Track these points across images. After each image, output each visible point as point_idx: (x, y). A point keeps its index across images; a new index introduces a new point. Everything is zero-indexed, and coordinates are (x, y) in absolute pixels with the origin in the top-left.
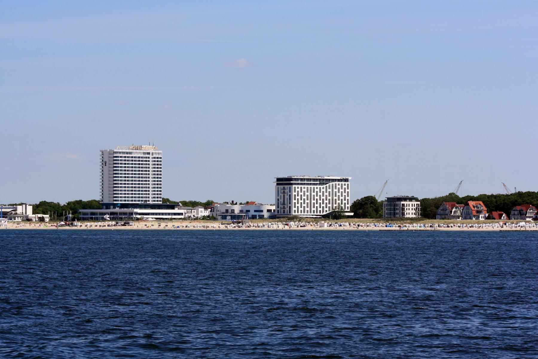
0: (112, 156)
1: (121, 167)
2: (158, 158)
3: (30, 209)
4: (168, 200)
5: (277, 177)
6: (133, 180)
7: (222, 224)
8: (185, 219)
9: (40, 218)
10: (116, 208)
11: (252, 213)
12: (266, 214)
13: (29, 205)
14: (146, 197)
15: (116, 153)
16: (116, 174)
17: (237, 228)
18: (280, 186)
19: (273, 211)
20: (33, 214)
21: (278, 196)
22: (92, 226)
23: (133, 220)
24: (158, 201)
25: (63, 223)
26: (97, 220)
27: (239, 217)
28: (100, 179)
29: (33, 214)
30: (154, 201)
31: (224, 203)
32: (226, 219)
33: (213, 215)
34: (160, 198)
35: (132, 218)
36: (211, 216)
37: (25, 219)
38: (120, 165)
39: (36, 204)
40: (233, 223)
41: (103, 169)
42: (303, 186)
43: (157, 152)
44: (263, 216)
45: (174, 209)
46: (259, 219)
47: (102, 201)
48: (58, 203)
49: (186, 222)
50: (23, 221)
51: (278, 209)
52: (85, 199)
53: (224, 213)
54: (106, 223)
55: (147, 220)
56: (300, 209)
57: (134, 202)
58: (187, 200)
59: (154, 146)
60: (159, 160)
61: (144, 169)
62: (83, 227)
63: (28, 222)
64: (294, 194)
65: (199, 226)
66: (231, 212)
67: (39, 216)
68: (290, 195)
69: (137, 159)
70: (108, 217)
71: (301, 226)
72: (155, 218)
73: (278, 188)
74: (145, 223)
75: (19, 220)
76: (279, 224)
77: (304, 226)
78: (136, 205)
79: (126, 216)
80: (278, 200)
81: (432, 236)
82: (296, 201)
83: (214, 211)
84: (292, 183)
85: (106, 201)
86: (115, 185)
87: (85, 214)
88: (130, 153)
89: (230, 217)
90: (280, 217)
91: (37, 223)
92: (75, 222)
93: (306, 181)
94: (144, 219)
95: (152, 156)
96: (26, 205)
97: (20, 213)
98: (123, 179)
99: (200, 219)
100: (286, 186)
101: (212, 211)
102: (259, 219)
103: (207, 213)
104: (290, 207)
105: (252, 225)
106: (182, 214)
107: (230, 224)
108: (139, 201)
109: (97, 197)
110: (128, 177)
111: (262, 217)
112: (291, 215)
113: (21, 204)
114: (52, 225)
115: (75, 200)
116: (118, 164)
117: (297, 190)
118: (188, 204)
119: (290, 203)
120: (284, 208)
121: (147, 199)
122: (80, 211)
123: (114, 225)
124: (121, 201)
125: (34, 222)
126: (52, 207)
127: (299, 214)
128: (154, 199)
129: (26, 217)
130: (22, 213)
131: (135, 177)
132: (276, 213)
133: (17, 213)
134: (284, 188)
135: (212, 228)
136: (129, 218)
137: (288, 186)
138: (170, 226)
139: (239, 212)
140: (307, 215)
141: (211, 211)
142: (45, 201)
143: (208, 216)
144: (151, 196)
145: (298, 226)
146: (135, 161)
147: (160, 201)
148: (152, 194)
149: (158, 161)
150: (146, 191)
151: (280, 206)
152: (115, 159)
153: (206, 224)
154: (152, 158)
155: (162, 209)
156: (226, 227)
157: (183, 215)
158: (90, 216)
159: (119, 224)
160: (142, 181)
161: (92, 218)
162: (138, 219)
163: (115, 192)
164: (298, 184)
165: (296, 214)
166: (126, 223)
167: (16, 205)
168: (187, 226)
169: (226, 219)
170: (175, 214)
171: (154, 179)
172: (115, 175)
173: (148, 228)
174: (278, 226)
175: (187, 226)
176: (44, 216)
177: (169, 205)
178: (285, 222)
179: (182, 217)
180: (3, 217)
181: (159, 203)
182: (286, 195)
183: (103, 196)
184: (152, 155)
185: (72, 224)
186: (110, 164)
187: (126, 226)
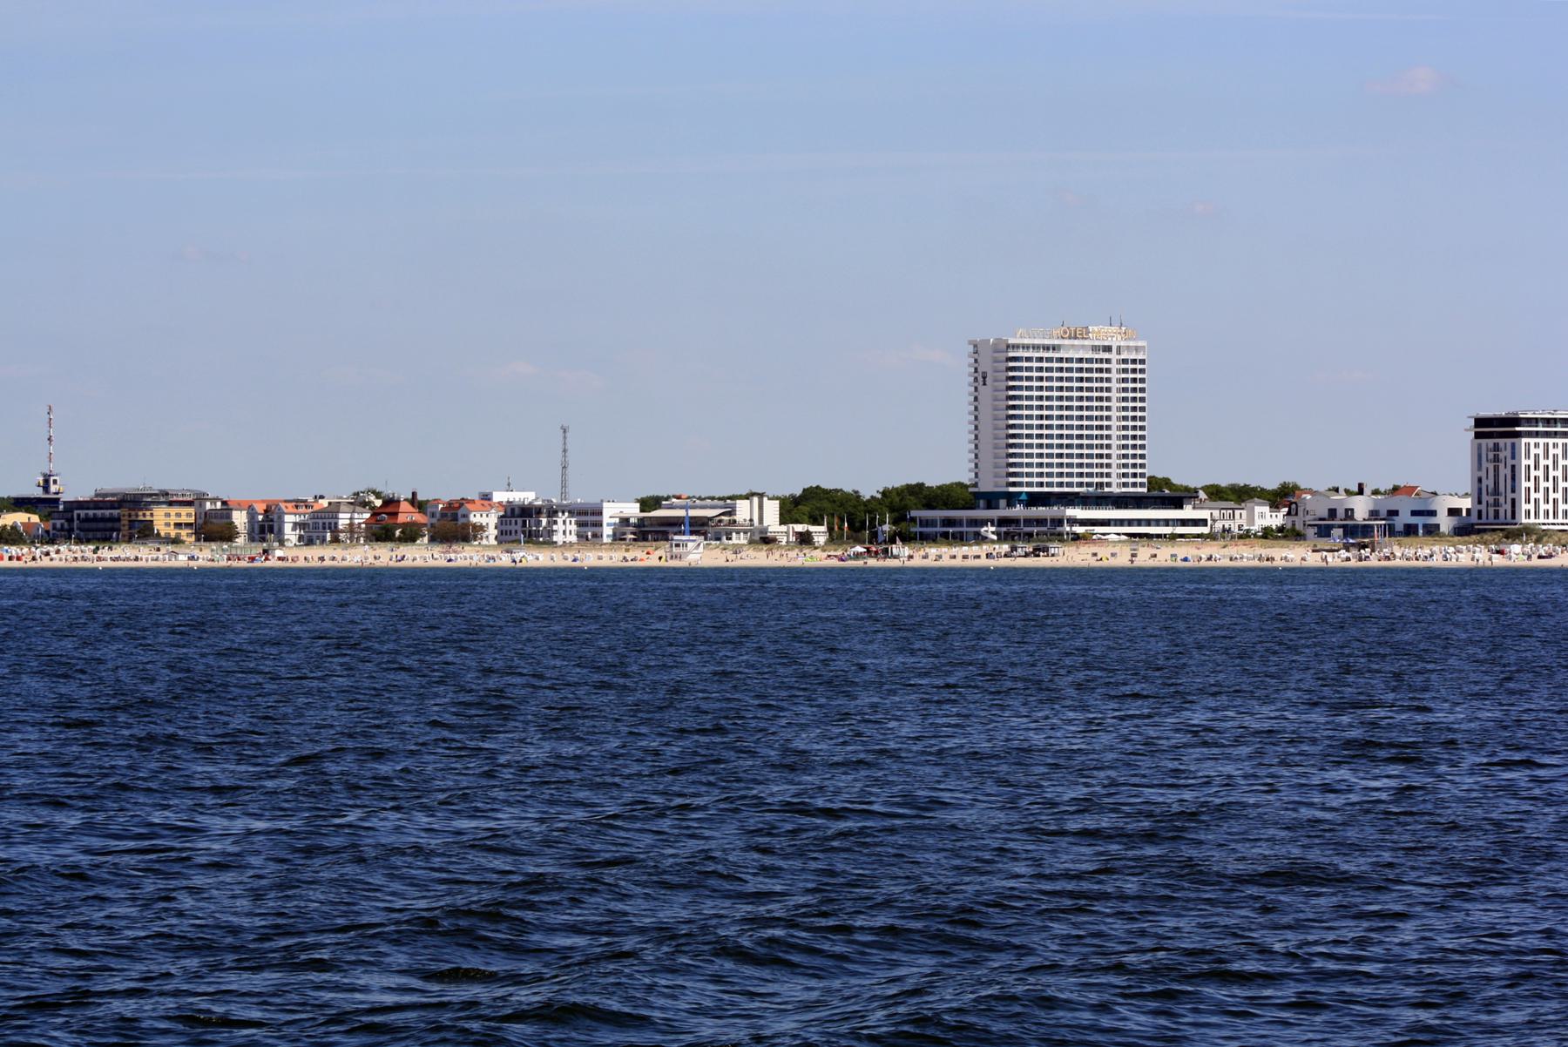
0: (1002, 356)
1: (1029, 388)
2: (1134, 361)
3: (772, 510)
4: (1166, 482)
5: (1475, 415)
6: (1062, 416)
7: (1314, 551)
8: (1212, 537)
9: (800, 534)
11: (1405, 518)
12: (1445, 523)
13: (769, 499)
14: (1102, 475)
15: (1015, 347)
16: (1014, 407)
17: (1353, 563)
18: (1484, 442)
19: (1464, 514)
20: (782, 522)
21: (1480, 468)
22: (940, 557)
23: (1062, 541)
24: (1134, 485)
25: (859, 549)
26: (962, 539)
27: (1366, 530)
28: (970, 423)
29: (782, 522)
30: (1125, 485)
31: (1330, 490)
32: (1329, 535)
33: (1294, 525)
34: (1142, 475)
35: (1060, 534)
36: (1289, 526)
37: (757, 537)
38: (1025, 393)
39: (792, 496)
40: (1347, 548)
41: (976, 394)
42: (1551, 441)
43: (1132, 343)
44: (1438, 526)
46: (1424, 535)
47: (976, 485)
48: (856, 492)
49: (1211, 546)
50: (751, 542)
51: (1480, 507)
52: (933, 481)
53: (1324, 519)
54: (986, 548)
55: (1102, 541)
56: (1543, 507)
57: (1066, 490)
58: (1224, 483)
59: (1123, 328)
60: (1139, 366)
61: (1095, 394)
62: (917, 562)
63: (765, 547)
64: (1524, 462)
65: (1247, 556)
66: (1343, 516)
67: (796, 530)
68: (1513, 467)
69: (1075, 365)
70: (993, 533)
71: (1540, 557)
73: (1480, 447)
74: (1094, 549)
75: (742, 540)
76: (1477, 549)
77: (1550, 556)
78: (1072, 497)
79: (1044, 529)
80: (1480, 480)
82: (1531, 484)
83: (1296, 514)
84: (1520, 432)
85: (986, 486)
86: (1011, 441)
88: (1054, 349)
89: (1341, 530)
90: (1485, 531)
91: (791, 549)
93: (1559, 425)
94: (1094, 537)
95: (1118, 357)
97: (745, 520)
98: (1035, 422)
99: (1255, 535)
100: (1501, 441)
101: (1293, 512)
102: (1424, 535)
103: (1276, 519)
104: (1513, 501)
105: (1398, 554)
106: (1203, 522)
107: (1337, 551)
108: (1080, 485)
109: (959, 472)
110: (1048, 417)
111: (1432, 531)
112: (1516, 524)
113: (748, 497)
114: (829, 556)
115: (904, 483)
116: (1020, 379)
117: (1531, 450)
119: (1513, 491)
120: (1496, 504)
121: (1105, 480)
122: (914, 513)
123: (1006, 556)
124: (1029, 484)
125: (781, 547)
126: (838, 503)
127: (1542, 520)
128: (1124, 480)
129: (761, 532)
130: (751, 520)
131: (1069, 418)
132: (1474, 519)
133: (735, 521)
134: (1496, 448)
135: (1284, 564)
136: (1053, 531)
137: (1509, 441)
138: (1163, 556)
139: (1367, 516)
140: (1563, 524)
141: (1289, 513)
142: (818, 487)
143: (1281, 529)
144: (1114, 471)
145: (1529, 557)
146: (1069, 370)
147: (1142, 485)
148: (1119, 466)
149: (1134, 399)
150: (1101, 428)
151: (1485, 498)
152: (1011, 364)
153: (1265, 552)
154: (1118, 362)
155: (1146, 507)
156: (1325, 559)
157: (1206, 525)
158: (939, 529)
159: (1019, 550)
160: (1088, 428)
161: (945, 535)
163: (1011, 460)
164: (1537, 434)
165: (1532, 520)
166: (1039, 550)
167: (733, 498)
168: (1211, 557)
169: (1329, 535)
170: (1184, 523)
171: (1124, 414)
173: (1099, 564)
174: (1474, 555)
175: (1211, 557)
176: (812, 528)
177: (1166, 495)
178: (1496, 544)
179: (1205, 530)
180: (692, 533)
182: (1502, 466)
183: (977, 470)
184: (1119, 352)
185: (886, 551)
186: (996, 381)
187: (1039, 556)
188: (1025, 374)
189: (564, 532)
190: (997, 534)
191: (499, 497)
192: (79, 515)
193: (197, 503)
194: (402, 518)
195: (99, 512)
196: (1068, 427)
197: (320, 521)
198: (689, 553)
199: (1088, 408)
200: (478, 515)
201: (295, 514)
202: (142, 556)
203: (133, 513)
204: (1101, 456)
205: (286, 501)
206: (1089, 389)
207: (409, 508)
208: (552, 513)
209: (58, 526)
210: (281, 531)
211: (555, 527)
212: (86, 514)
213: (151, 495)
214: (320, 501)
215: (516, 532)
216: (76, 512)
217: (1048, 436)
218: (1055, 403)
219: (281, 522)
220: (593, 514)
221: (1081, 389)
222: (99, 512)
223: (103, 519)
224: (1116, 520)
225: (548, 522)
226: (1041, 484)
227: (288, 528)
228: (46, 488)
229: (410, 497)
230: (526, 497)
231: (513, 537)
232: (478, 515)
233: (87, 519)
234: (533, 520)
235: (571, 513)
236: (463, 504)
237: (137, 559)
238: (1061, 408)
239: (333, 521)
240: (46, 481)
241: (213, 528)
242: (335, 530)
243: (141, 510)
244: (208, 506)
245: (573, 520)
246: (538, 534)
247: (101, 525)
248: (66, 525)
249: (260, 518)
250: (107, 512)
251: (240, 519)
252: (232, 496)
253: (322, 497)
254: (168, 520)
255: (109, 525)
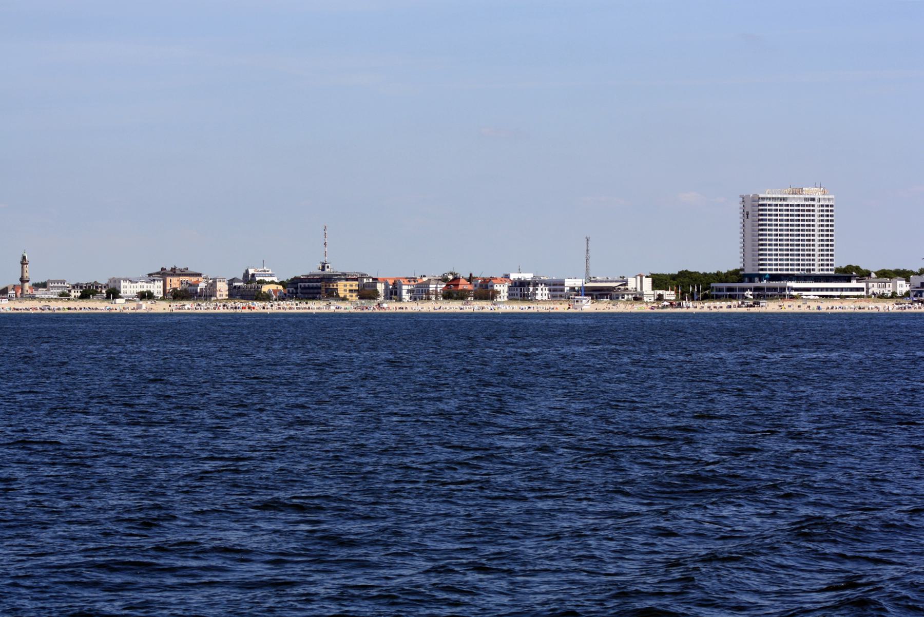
0: (756, 203)
2: (827, 206)
10: (763, 281)
15: (764, 199)
16: (762, 230)
20: (653, 290)
22: (703, 307)
24: (827, 270)
30: (822, 270)
43: (826, 197)
45: (850, 281)
47: (742, 270)
59: (822, 189)
60: (830, 208)
61: (806, 223)
65: (890, 307)
70: (751, 295)
72: (818, 296)
79: (776, 293)
81: (717, 319)
85: (748, 271)
87: (720, 290)
92: (684, 302)
95: (818, 204)
96: (641, 277)
105: (691, 306)
108: (798, 270)
110: (781, 235)
118: (888, 273)
121: (811, 267)
122: (712, 285)
124: (770, 270)
133: (627, 289)
135: (840, 310)
142: (686, 271)
147: (831, 270)
154: (818, 206)
155: (831, 282)
162: (792, 297)
170: (852, 289)
172: (761, 232)
180: (586, 295)
181: (830, 272)
184: (819, 201)
186: (753, 216)
187: (754, 307)
188: (768, 213)
189: (542, 295)
190: (754, 296)
191: (514, 276)
192: (301, 286)
193: (359, 279)
194: (460, 287)
195: (311, 284)
196: (791, 240)
197: (421, 289)
198: (584, 305)
199: (802, 230)
200: (498, 286)
201: (408, 285)
202: (333, 307)
203: (327, 284)
204: (809, 255)
205: (403, 278)
206: (803, 220)
207: (465, 282)
208: (536, 284)
209: (291, 291)
210: (401, 293)
211: (537, 292)
212: (304, 285)
213: (337, 275)
214: (423, 278)
215: (517, 294)
216: (299, 284)
217: (780, 245)
218: (784, 228)
219: (401, 289)
220: (560, 285)
221: (798, 220)
222: (311, 284)
223: (313, 288)
224: (814, 288)
225: (534, 289)
226: (777, 270)
227: (404, 293)
228: (323, 269)
229: (468, 276)
230: (528, 276)
231: (515, 297)
232: (498, 286)
233: (305, 288)
234: (525, 288)
235: (546, 285)
236: (490, 280)
237: (309, 308)
238: (787, 230)
239: (427, 289)
240: (323, 267)
241: (367, 292)
242: (428, 293)
243: (331, 283)
244: (365, 281)
245: (547, 288)
246: (528, 296)
247: (312, 291)
248: (294, 291)
249: (391, 287)
250: (315, 284)
251: (380, 287)
252: (396, 275)
253: (424, 276)
254: (345, 288)
255: (316, 291)
